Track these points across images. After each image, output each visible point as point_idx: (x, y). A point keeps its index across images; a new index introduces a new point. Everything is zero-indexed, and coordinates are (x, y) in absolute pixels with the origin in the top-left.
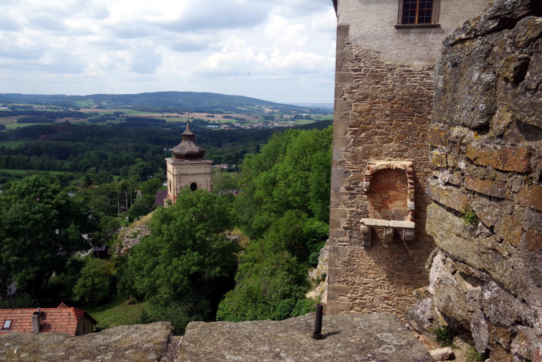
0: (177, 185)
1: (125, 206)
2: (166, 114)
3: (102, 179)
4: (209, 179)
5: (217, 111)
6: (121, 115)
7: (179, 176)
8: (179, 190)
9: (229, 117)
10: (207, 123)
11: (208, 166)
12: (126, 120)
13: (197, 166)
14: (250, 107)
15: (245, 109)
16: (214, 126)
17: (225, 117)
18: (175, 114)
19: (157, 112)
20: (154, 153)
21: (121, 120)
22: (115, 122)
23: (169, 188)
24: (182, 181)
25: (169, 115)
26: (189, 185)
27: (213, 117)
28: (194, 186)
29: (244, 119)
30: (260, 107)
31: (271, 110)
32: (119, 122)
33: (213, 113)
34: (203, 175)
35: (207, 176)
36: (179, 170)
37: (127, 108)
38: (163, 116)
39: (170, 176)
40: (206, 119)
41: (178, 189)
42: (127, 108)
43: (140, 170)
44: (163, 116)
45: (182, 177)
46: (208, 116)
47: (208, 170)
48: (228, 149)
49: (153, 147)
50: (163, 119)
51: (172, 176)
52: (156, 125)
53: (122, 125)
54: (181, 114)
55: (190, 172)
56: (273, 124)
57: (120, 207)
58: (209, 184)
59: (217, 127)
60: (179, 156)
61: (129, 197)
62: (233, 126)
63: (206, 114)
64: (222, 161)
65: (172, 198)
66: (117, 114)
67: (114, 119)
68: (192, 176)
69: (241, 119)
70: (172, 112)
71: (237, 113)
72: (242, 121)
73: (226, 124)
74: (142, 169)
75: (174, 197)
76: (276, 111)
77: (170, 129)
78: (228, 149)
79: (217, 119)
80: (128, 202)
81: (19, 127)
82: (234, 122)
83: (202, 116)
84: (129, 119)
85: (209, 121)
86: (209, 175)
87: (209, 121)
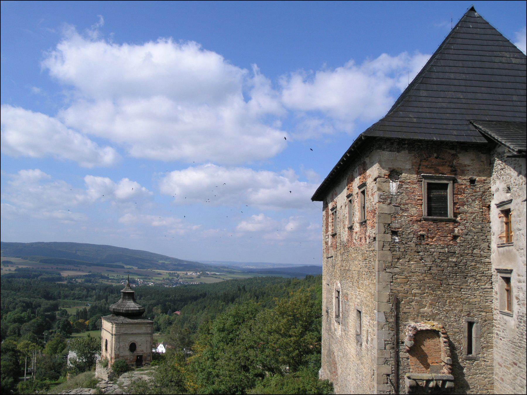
4: (149, 339)
7: (118, 336)
11: (148, 325)
24: (120, 340)
26: (128, 347)
28: (133, 347)
49: (46, 303)
51: (110, 335)
75: (111, 358)
86: (149, 335)
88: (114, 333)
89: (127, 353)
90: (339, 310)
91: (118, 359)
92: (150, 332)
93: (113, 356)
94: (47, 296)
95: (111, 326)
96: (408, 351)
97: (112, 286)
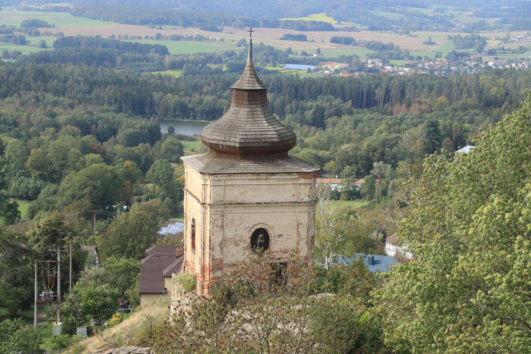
0: (212, 234)
1: (55, 289)
2: (168, 30)
3: (371, 206)
4: (304, 219)
5: (314, 23)
6: (41, 30)
7: (220, 207)
8: (217, 249)
9: (348, 41)
10: (285, 58)
11: (302, 181)
12: (56, 44)
13: (273, 181)
14: (412, 9)
15: (396, 16)
16: (305, 67)
17: (335, 40)
18: (195, 32)
19: (144, 22)
20: (133, 140)
21: (44, 45)
22: (26, 50)
23: (188, 241)
24: (227, 222)
25: (180, 31)
26: (247, 236)
27: (302, 38)
28: (260, 239)
29: (391, 46)
30: (443, 10)
31: (477, 20)
32: (36, 50)
33: (301, 28)
34: (291, 210)
35: (298, 209)
36: (220, 190)
37: (57, 10)
38: (159, 37)
39: (192, 207)
40: (282, 46)
41: (217, 245)
42: (57, 10)
43: (95, 188)
44: (159, 37)
45: (228, 210)
46: (288, 37)
47: (304, 194)
48: (348, 134)
49: (132, 124)
50: (161, 43)
51: (199, 207)
52: (140, 60)
53: (44, 58)
54: (213, 29)
55: (251, 197)
56: (480, 60)
57: (40, 292)
58: (304, 234)
59: (312, 68)
60: (219, 151)
61: (64, 264)
62: (362, 68)
63: (282, 32)
64: (327, 166)
65: (198, 270)
66: (33, 26)
67: (23, 42)
68: (257, 210)
69: (384, 47)
70: (187, 24)
71: (373, 28)
72: (385, 51)
73: (341, 60)
74: (98, 183)
75: (203, 269)
76: (491, 21)
77: (176, 74)
78: (348, 134)
79: (315, 46)
80: (62, 281)
81: (41, 52)
82: (362, 54)
83: (269, 38)
84: (64, 42)
85: (289, 51)
86: (305, 209)
87: (289, 51)
88: (208, 201)
89: (240, 254)
90: (282, 173)
91: (219, 274)
92: (307, 199)
93: (207, 263)
94: (140, 106)
95: (202, 182)
96: (324, 128)
97: (131, 43)
